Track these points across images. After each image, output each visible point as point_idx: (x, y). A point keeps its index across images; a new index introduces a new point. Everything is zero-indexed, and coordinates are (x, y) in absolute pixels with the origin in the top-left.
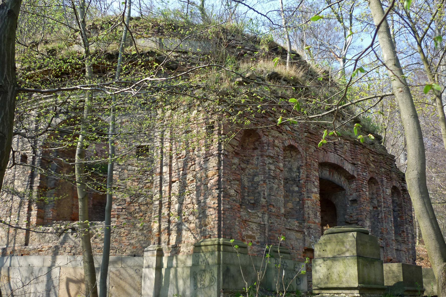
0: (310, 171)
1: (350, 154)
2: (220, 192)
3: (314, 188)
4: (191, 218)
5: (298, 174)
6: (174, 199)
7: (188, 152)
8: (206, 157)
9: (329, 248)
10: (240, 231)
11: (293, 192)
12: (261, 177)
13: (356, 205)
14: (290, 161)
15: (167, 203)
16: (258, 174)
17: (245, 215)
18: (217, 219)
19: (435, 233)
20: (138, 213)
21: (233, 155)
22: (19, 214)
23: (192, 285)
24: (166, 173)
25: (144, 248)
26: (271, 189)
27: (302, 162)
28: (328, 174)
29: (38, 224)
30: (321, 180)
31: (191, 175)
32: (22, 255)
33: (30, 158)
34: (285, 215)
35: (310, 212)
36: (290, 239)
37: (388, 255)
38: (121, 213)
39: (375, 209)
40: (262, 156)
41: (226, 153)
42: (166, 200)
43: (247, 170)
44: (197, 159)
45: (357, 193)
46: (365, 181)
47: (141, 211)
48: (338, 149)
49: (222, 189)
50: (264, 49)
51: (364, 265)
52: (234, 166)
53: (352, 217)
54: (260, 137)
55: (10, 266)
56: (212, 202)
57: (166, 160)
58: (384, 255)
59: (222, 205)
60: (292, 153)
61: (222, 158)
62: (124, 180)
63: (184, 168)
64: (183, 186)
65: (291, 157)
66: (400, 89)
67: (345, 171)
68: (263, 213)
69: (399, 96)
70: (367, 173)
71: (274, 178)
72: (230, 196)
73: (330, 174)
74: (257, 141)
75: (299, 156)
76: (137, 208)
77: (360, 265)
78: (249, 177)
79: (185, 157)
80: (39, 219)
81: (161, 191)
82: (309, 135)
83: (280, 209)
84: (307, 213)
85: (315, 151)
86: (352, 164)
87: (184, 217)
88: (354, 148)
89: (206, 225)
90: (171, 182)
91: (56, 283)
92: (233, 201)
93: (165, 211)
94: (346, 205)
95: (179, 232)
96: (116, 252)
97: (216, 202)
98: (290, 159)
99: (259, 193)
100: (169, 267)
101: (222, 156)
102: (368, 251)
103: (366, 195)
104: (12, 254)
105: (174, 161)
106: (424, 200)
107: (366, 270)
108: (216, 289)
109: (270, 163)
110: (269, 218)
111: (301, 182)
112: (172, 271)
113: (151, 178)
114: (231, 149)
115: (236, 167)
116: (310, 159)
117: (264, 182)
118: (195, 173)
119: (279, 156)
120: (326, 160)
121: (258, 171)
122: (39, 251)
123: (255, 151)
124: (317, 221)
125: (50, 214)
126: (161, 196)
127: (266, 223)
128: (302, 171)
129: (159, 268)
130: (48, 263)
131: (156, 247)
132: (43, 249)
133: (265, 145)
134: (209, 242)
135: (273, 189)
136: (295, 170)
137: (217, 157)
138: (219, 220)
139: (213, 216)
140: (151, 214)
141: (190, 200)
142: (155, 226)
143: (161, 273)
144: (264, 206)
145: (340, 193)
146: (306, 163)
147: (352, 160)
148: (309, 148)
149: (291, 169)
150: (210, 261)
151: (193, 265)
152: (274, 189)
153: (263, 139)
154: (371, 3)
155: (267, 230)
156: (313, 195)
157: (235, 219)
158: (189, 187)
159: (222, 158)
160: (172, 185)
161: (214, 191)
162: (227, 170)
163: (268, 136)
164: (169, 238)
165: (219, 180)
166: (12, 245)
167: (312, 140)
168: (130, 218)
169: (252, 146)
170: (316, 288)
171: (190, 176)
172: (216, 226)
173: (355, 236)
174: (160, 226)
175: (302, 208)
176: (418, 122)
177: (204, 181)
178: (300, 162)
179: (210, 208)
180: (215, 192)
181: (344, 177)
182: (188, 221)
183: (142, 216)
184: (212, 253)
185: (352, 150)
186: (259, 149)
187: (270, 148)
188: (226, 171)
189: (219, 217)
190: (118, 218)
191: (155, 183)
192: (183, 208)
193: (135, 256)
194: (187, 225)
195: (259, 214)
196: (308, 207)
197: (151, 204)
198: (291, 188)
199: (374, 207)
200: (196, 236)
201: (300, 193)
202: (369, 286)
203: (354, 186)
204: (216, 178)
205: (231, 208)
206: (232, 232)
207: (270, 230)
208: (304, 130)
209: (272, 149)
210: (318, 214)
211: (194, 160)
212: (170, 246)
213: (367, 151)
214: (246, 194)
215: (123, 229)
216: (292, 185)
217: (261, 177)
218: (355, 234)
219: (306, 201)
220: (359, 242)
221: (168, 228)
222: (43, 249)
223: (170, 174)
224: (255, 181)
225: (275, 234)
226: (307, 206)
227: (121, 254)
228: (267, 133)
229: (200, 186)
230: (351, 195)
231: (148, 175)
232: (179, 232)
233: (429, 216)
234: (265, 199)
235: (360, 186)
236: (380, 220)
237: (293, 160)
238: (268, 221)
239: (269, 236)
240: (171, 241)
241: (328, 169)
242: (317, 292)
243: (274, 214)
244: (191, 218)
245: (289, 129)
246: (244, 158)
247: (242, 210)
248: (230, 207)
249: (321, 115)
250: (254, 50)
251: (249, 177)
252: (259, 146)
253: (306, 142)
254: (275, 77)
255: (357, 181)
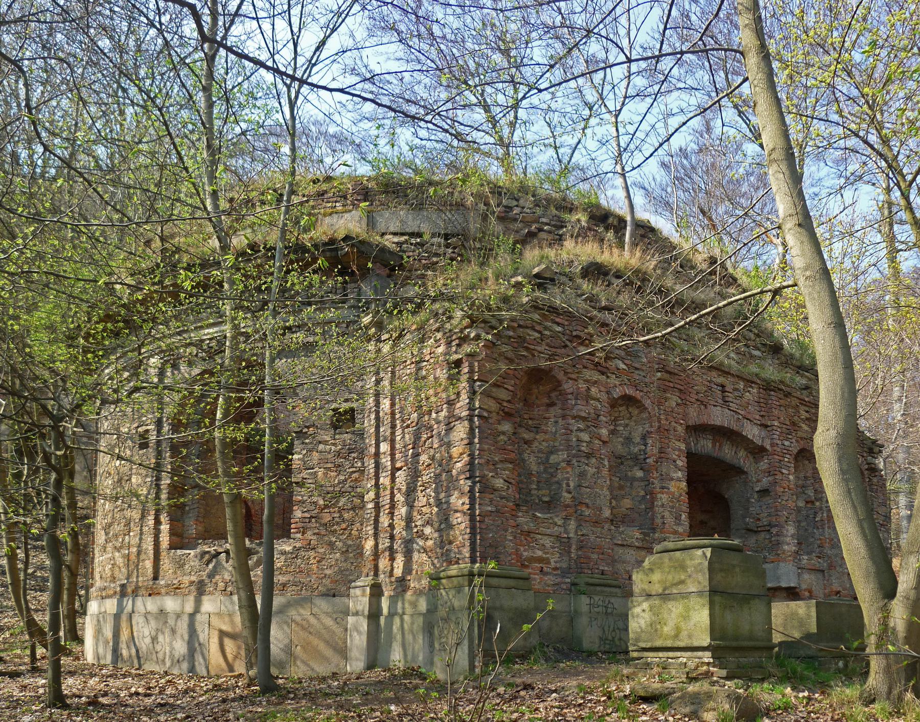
0: (667, 441)
1: (758, 408)
2: (474, 483)
3: (676, 472)
4: (428, 530)
5: (643, 447)
6: (400, 498)
7: (420, 417)
8: (450, 423)
9: (656, 577)
10: (518, 550)
11: (634, 479)
12: (563, 455)
13: (768, 498)
14: (627, 425)
15: (387, 506)
16: (558, 450)
17: (527, 522)
18: (468, 531)
19: (867, 546)
20: (338, 523)
21: (500, 418)
22: (141, 530)
23: (426, 645)
24: (384, 453)
25: (351, 581)
26: (582, 475)
27: (651, 426)
28: (710, 445)
29: (173, 547)
30: (691, 457)
31: (426, 456)
32: (150, 595)
33: (153, 437)
34: (612, 521)
35: (667, 514)
36: (624, 562)
37: (831, 584)
38: (309, 525)
39: (809, 506)
40: (564, 417)
41: (485, 414)
42: (385, 500)
43: (536, 444)
44: (435, 426)
45: (770, 478)
46: (788, 456)
47: (344, 521)
48: (730, 399)
49: (477, 479)
50: (579, 220)
51: (725, 607)
52: (502, 437)
53: (759, 519)
54: (559, 383)
55: (133, 612)
56: (459, 501)
57: (385, 430)
58: (824, 585)
59: (477, 507)
60: (630, 410)
61: (477, 423)
62: (313, 468)
63: (414, 443)
64: (415, 475)
65: (630, 418)
66: (808, 273)
67: (745, 439)
68: (566, 519)
69: (805, 287)
70: (794, 441)
71: (588, 456)
72: (495, 490)
73: (714, 445)
74: (554, 390)
75: (644, 415)
76: (336, 515)
77: (717, 607)
78: (540, 455)
79: (417, 424)
80: (173, 538)
81: (377, 485)
82: (667, 376)
83: (600, 509)
84: (659, 516)
85: (678, 404)
86: (761, 425)
87: (415, 530)
88: (766, 397)
89: (450, 543)
90: (395, 470)
91: (202, 637)
92: (502, 498)
93: (384, 521)
94: (748, 500)
95: (408, 554)
96: (301, 590)
97: (467, 501)
98: (627, 422)
99: (558, 483)
100: (391, 615)
101: (476, 419)
102: (738, 581)
103: (789, 481)
104: (135, 593)
105: (399, 432)
106: (847, 485)
107: (729, 617)
108: (467, 651)
109: (579, 430)
110: (579, 526)
111: (648, 461)
112: (397, 620)
113: (359, 464)
114: (493, 405)
115: (506, 439)
116: (667, 419)
117: (569, 463)
118: (432, 452)
119: (599, 416)
120: (704, 419)
121: (557, 444)
122: (175, 590)
123: (552, 409)
124: (680, 530)
125: (192, 528)
126: (378, 495)
127: (571, 535)
128: (650, 441)
129: (374, 615)
130: (189, 607)
131: (369, 580)
132: (182, 586)
133: (570, 396)
134: (454, 570)
135: (586, 475)
136: (638, 440)
137: (466, 422)
138: (473, 533)
139: (463, 526)
140: (362, 525)
141: (425, 499)
142: (369, 545)
143: (378, 625)
144: (567, 506)
145: (738, 478)
146: (659, 427)
147: (760, 418)
148: (666, 399)
149: (628, 440)
150: (456, 604)
151: (428, 611)
152: (589, 475)
153: (565, 386)
154: (758, 105)
155: (574, 547)
156: (673, 483)
157: (506, 531)
158: (424, 478)
159: (477, 423)
160: (397, 475)
161: (462, 482)
162: (488, 444)
163: (576, 380)
164: (392, 565)
165: (471, 463)
166: (135, 580)
167: (671, 385)
168: (323, 532)
169: (546, 400)
170: (635, 648)
171: (424, 458)
172: (467, 544)
173: (709, 555)
174: (376, 545)
175: (652, 507)
176: (844, 337)
177: (445, 465)
178: (647, 425)
179: (456, 511)
180: (465, 485)
181: (745, 449)
182: (421, 535)
183: (345, 529)
184: (459, 589)
185: (762, 400)
186: (559, 405)
187: (579, 402)
188: (486, 447)
189: (473, 528)
190: (303, 533)
191: (366, 473)
192: (415, 514)
193: (334, 596)
194: (421, 543)
195: (556, 520)
196: (663, 505)
197: (361, 508)
198: (629, 474)
199: (807, 502)
200: (436, 561)
201: (647, 481)
202: (734, 644)
203: (764, 464)
204: (466, 459)
205: (498, 511)
206: (500, 553)
207: (580, 548)
208: (657, 366)
209: (584, 403)
210: (683, 516)
211: (431, 428)
212: (393, 579)
213: (795, 402)
214: (535, 487)
215: (313, 552)
216: (631, 467)
217: (563, 455)
218: (708, 552)
219: (659, 496)
220: (717, 566)
221: (391, 549)
222: (182, 586)
223: (393, 455)
224: (551, 462)
225: (590, 554)
226: (660, 504)
227: (309, 593)
228: (573, 376)
229: (440, 475)
230: (758, 481)
231: (354, 458)
232: (408, 554)
233: (858, 515)
234: (570, 493)
235: (777, 464)
236: (819, 524)
237: (633, 423)
238: (576, 532)
239: (579, 557)
240: (395, 571)
241: (711, 437)
242: (635, 655)
243: (587, 519)
244: (428, 530)
245: (625, 367)
246: (530, 422)
247: (520, 514)
248: (494, 509)
249: (659, 334)
250: (558, 223)
251: (540, 455)
252: (558, 399)
253: (659, 388)
254: (595, 271)
255: (770, 457)
